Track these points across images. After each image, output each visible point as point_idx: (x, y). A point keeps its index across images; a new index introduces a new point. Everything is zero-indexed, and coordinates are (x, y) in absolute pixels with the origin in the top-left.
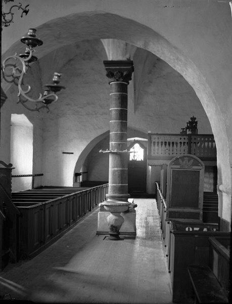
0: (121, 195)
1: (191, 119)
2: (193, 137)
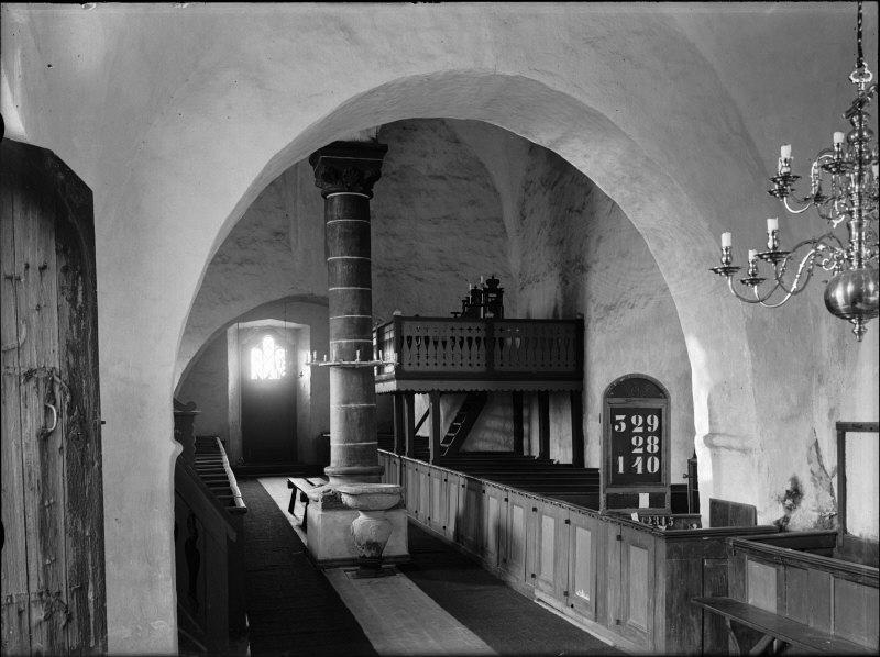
0: (368, 468)
1: (488, 282)
2: (497, 326)
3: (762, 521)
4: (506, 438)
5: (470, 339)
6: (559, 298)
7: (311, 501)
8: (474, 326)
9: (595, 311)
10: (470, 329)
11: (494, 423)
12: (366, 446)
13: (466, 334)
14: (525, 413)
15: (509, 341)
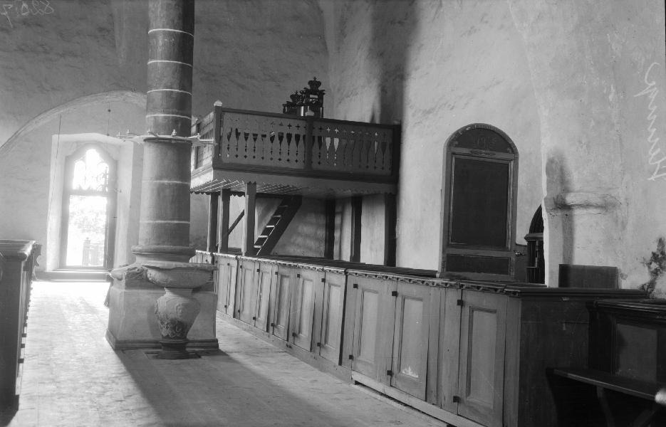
0: (178, 248)
1: (310, 83)
2: (317, 125)
3: (625, 285)
4: (317, 244)
5: (289, 136)
6: (378, 107)
7: (115, 279)
8: (294, 123)
9: (413, 115)
10: (290, 126)
11: (306, 229)
12: (177, 224)
13: (286, 131)
14: (338, 220)
15: (328, 140)
